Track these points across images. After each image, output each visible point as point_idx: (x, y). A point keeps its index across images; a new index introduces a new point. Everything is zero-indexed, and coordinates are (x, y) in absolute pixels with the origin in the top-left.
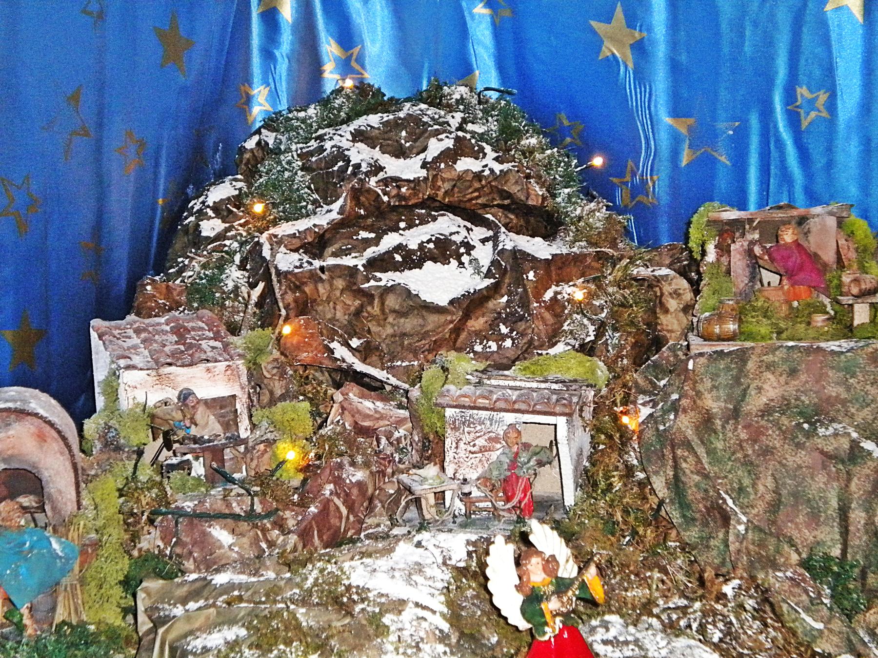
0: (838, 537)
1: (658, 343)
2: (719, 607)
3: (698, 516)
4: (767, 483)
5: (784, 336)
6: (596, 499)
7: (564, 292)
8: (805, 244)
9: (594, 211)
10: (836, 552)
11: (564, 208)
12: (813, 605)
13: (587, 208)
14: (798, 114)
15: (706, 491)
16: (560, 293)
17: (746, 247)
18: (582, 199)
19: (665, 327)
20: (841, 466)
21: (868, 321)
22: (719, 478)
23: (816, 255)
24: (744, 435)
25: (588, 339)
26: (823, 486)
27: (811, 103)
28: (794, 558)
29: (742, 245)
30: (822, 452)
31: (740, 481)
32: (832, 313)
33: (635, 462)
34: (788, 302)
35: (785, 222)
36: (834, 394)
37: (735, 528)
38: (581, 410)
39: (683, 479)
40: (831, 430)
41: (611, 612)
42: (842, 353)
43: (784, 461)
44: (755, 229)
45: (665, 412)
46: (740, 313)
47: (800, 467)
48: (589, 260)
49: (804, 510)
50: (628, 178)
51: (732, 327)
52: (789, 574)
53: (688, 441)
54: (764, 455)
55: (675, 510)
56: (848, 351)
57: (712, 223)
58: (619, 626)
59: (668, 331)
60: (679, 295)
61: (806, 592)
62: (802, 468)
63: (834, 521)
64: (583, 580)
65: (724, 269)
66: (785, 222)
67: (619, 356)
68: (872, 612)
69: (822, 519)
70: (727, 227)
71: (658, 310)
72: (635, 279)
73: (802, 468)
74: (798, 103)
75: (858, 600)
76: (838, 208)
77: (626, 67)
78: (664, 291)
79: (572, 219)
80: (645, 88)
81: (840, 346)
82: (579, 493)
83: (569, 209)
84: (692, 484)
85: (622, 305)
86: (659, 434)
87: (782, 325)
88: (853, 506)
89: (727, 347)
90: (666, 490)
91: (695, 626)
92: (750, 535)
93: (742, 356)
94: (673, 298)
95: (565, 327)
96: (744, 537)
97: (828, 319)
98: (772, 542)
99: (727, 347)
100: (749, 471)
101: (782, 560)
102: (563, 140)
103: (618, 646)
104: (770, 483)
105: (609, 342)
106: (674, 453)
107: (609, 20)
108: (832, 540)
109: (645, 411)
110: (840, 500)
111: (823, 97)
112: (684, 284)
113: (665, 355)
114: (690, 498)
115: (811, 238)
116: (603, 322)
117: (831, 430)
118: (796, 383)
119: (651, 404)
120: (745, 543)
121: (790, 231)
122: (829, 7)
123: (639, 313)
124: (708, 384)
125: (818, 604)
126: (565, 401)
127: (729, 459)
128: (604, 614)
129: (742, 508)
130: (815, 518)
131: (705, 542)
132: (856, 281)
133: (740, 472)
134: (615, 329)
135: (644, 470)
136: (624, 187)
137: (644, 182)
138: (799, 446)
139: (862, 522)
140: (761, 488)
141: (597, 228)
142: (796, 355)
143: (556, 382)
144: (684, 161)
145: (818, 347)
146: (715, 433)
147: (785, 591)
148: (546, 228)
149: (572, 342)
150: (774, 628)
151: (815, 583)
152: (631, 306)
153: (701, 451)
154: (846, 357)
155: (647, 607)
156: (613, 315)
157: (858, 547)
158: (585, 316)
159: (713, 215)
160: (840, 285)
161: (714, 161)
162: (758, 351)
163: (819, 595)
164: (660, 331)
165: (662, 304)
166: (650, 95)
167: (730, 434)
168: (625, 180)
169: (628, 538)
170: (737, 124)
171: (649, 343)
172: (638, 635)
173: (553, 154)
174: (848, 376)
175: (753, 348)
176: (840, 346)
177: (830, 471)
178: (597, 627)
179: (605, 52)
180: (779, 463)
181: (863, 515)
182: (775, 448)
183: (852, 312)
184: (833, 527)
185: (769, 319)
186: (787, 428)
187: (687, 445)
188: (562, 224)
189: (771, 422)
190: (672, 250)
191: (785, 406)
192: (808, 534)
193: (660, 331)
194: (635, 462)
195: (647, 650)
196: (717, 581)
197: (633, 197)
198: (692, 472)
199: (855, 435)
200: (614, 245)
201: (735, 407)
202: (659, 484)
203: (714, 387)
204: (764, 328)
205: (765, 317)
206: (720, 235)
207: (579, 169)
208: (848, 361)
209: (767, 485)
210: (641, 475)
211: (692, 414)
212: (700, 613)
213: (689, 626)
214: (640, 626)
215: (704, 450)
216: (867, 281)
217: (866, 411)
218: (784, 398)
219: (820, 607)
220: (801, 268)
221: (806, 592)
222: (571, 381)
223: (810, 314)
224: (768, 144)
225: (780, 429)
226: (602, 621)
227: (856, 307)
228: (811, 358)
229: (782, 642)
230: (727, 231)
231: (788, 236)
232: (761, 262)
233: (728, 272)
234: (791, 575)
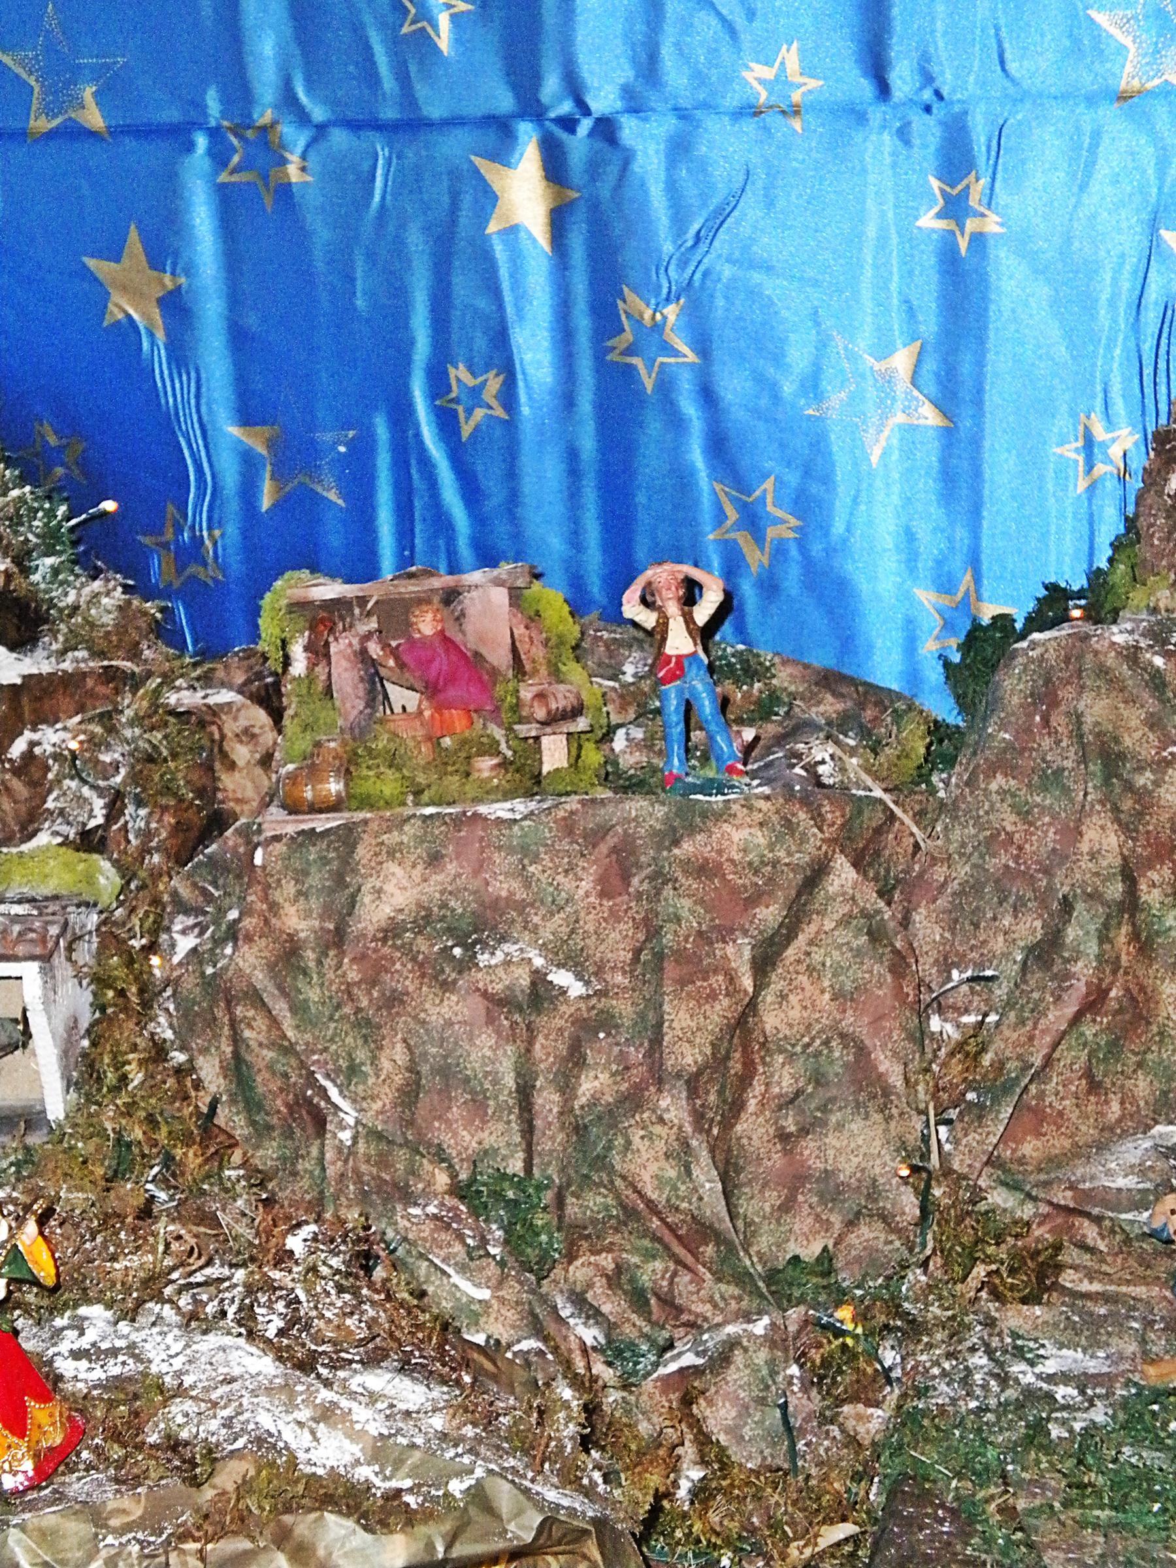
0: (517, 1139)
1: (218, 822)
2: (276, 1275)
3: (275, 1121)
4: (395, 1056)
5: (425, 797)
6: (100, 1105)
7: (45, 741)
8: (458, 638)
9: (97, 595)
10: (516, 1166)
11: (46, 592)
12: (472, 1259)
13: (86, 591)
14: (455, 414)
15: (286, 1075)
16: (39, 744)
17: (357, 647)
18: (77, 576)
19: (231, 795)
20: (517, 1017)
21: (566, 765)
22: (313, 1052)
23: (477, 654)
24: (353, 975)
25: (92, 824)
26: (489, 1053)
27: (475, 393)
28: (442, 1179)
29: (350, 645)
30: (485, 994)
31: (350, 1055)
32: (509, 753)
33: (169, 1035)
34: (434, 741)
35: (421, 601)
36: (504, 894)
37: (335, 1136)
38: (70, 949)
39: (248, 1058)
40: (499, 956)
41: (89, 1302)
42: (515, 820)
43: (422, 1015)
44: (369, 614)
45: (218, 942)
46: (349, 762)
47: (449, 1023)
48: (90, 683)
49: (461, 1096)
50: (169, 535)
51: (334, 787)
52: (432, 1209)
53: (256, 990)
54: (390, 1008)
55: (238, 1113)
56: (525, 818)
57: (299, 607)
58: (101, 1324)
59: (238, 801)
60: (253, 736)
61: (461, 1237)
62: (452, 1024)
63: (510, 1113)
64: (16, 1246)
65: (320, 687)
66: (421, 601)
67: (145, 851)
68: (578, 1263)
69: (490, 1112)
70: (323, 614)
71: (217, 766)
72: (172, 713)
73: (452, 1024)
74: (453, 395)
75: (550, 1243)
76: (509, 573)
77: (151, 335)
78: (226, 731)
79: (61, 610)
80: (188, 374)
81: (512, 810)
82: (73, 1095)
83: (54, 594)
84: (262, 1065)
85: (150, 759)
86: (208, 983)
87: (421, 779)
88: (538, 1084)
89: (322, 823)
90: (221, 1080)
91: (231, 1311)
92: (362, 1147)
93: (347, 837)
94: (241, 742)
95: (50, 804)
96: (352, 1151)
97: (499, 765)
98: (401, 1157)
99: (322, 823)
100: (365, 1037)
101: (420, 1186)
102: (49, 471)
103: (98, 1359)
104: (400, 1054)
105: (130, 825)
106: (230, 1013)
107: (116, 256)
108: (508, 1144)
109: (185, 944)
110: (518, 1074)
111: (494, 384)
112: (261, 716)
113: (231, 843)
114: (261, 1090)
115: (469, 627)
116: (118, 792)
117: (499, 956)
118: (439, 878)
119: (196, 931)
120: (351, 1162)
121: (430, 616)
122: (492, 228)
123: (180, 772)
124: (290, 888)
125: (481, 1257)
126: (33, 935)
127: (331, 1018)
128: (76, 1306)
129: (354, 1101)
130: (478, 1105)
131: (289, 1165)
132: (541, 696)
133: (349, 1040)
134: (139, 803)
135: (183, 1048)
136: (163, 552)
137: (198, 542)
138: (447, 986)
139: (555, 1110)
140: (386, 1064)
141: (103, 626)
142: (438, 830)
143: (20, 902)
144: (266, 503)
145: (475, 814)
146: (305, 974)
147: (424, 1239)
148: (19, 629)
149: (64, 829)
150: (373, 1304)
151: (477, 1220)
152: (165, 760)
153: (280, 1007)
154: (522, 828)
155: (152, 1286)
156: (134, 777)
157: (551, 1151)
158: (85, 782)
159: (298, 593)
160: (516, 707)
161: (317, 499)
162: (374, 826)
163: (484, 1242)
164: (223, 802)
165: (224, 755)
166: (198, 388)
167: (331, 975)
168: (163, 539)
169: (156, 1169)
170: (351, 434)
171: (203, 824)
172: (136, 1337)
173: (21, 499)
174: (526, 861)
175: (365, 822)
176: (512, 810)
177: (500, 1025)
178: (63, 1329)
179: (115, 314)
180: (415, 1018)
181: (556, 1097)
182: (407, 994)
183: (539, 750)
184: (509, 1122)
185: (399, 769)
186: (426, 958)
187: (255, 998)
188: (46, 621)
189: (397, 948)
190: (248, 658)
191: (424, 920)
192: (468, 1138)
193: (223, 802)
194: (169, 1035)
195: (150, 1362)
196: (276, 1231)
197: (179, 571)
198: (261, 1045)
199: (539, 962)
200: (134, 654)
201: (336, 928)
202: (210, 1071)
203: (300, 893)
204: (389, 785)
205: (390, 767)
206: (312, 629)
207: (73, 522)
208: (526, 836)
209: (397, 1058)
210: (179, 1057)
211: (263, 942)
212: (240, 1289)
213: (224, 1314)
214: (142, 1320)
215: (286, 1006)
216: (560, 696)
217: (558, 918)
218: (420, 906)
219: (484, 1262)
220: (452, 679)
221: (461, 1237)
222: (46, 899)
223: (468, 758)
224: (407, 464)
225: (414, 959)
226: (73, 1317)
227: (545, 740)
228: (462, 834)
229: (387, 1326)
230: (323, 620)
231: (426, 625)
232: (383, 672)
233: (328, 692)
234: (436, 1211)
